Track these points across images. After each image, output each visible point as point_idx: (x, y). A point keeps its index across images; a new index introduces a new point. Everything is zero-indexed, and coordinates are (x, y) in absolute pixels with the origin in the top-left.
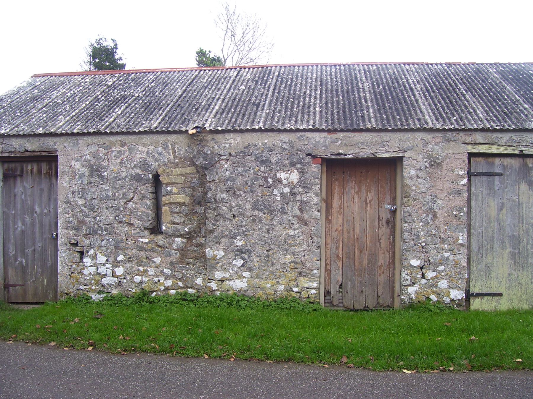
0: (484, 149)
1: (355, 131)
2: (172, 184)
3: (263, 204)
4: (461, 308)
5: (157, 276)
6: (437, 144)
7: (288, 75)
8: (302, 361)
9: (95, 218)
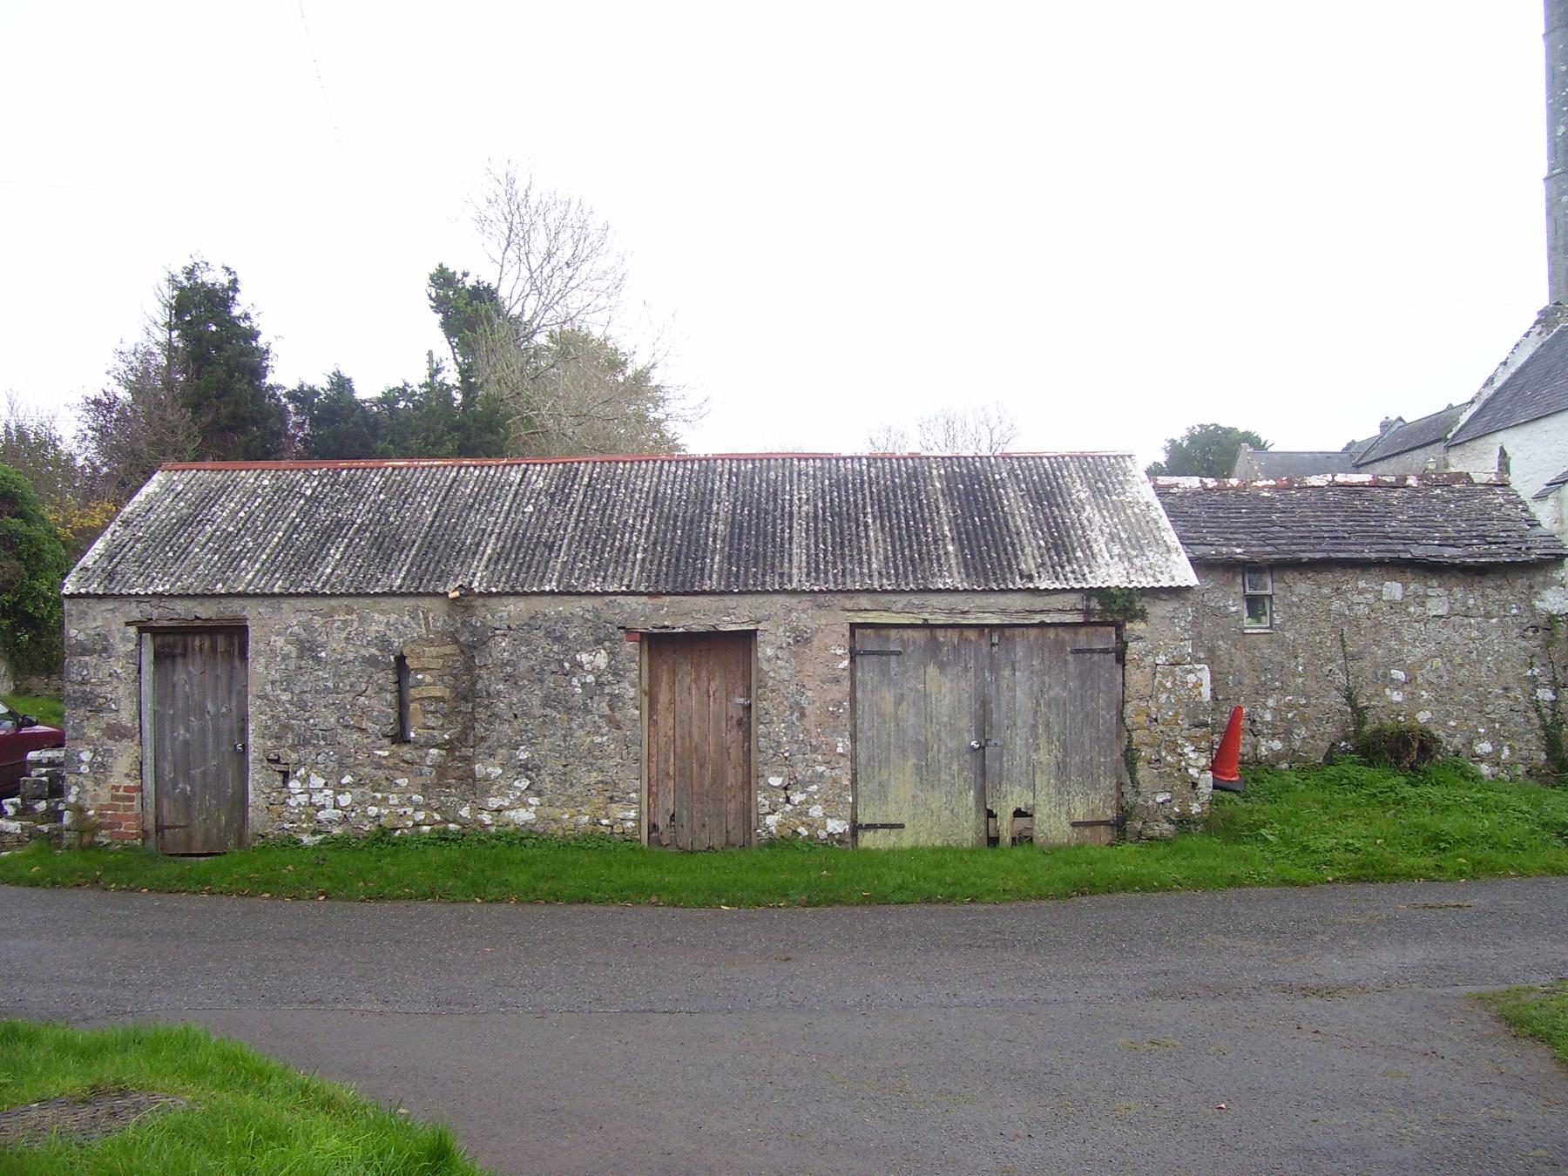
0: (871, 618)
1: (686, 594)
2: (424, 670)
3: (557, 699)
4: (843, 846)
5: (403, 806)
6: (804, 611)
7: (605, 482)
8: (600, 902)
9: (307, 720)
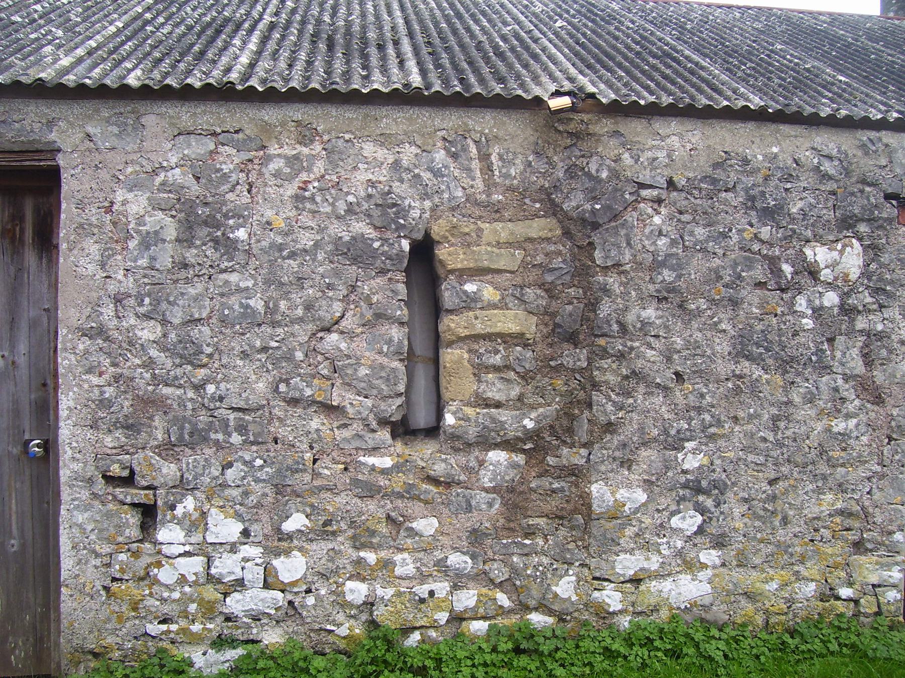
5: (423, 578)
9: (199, 387)
